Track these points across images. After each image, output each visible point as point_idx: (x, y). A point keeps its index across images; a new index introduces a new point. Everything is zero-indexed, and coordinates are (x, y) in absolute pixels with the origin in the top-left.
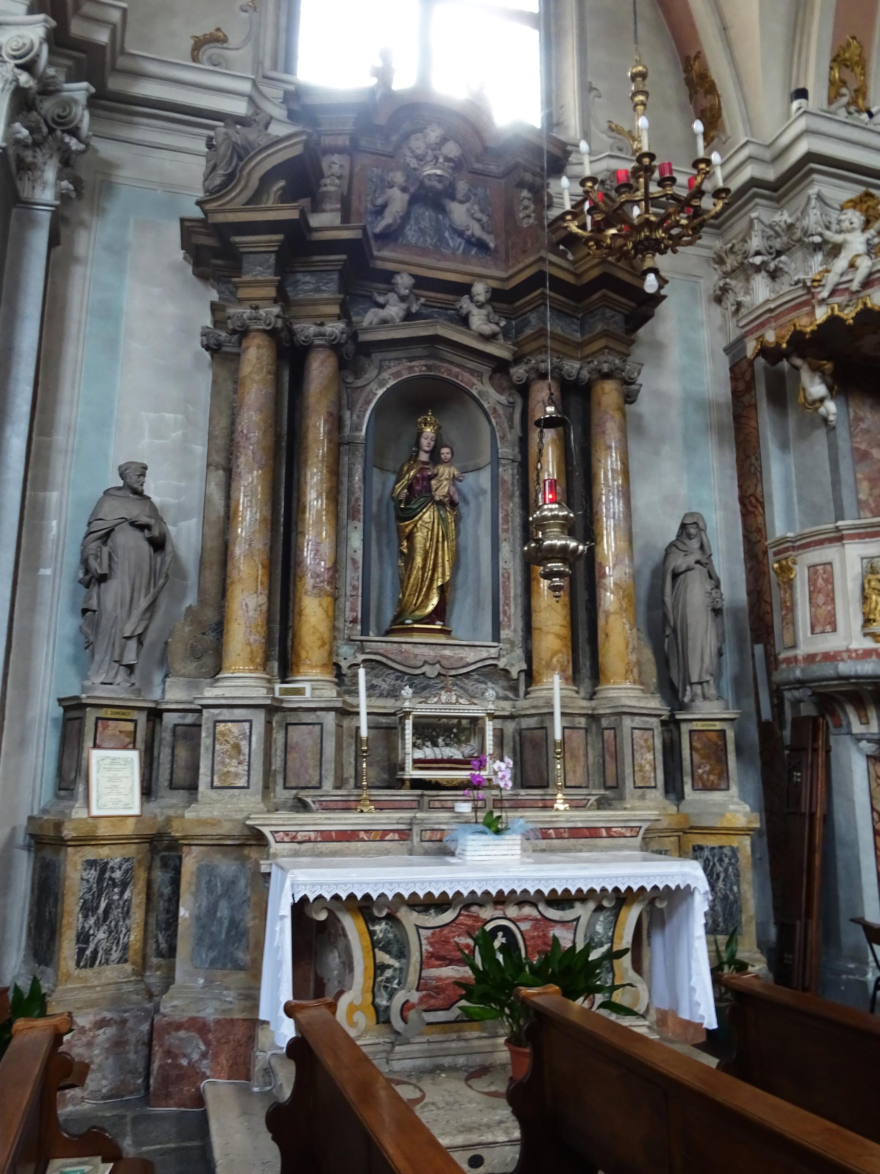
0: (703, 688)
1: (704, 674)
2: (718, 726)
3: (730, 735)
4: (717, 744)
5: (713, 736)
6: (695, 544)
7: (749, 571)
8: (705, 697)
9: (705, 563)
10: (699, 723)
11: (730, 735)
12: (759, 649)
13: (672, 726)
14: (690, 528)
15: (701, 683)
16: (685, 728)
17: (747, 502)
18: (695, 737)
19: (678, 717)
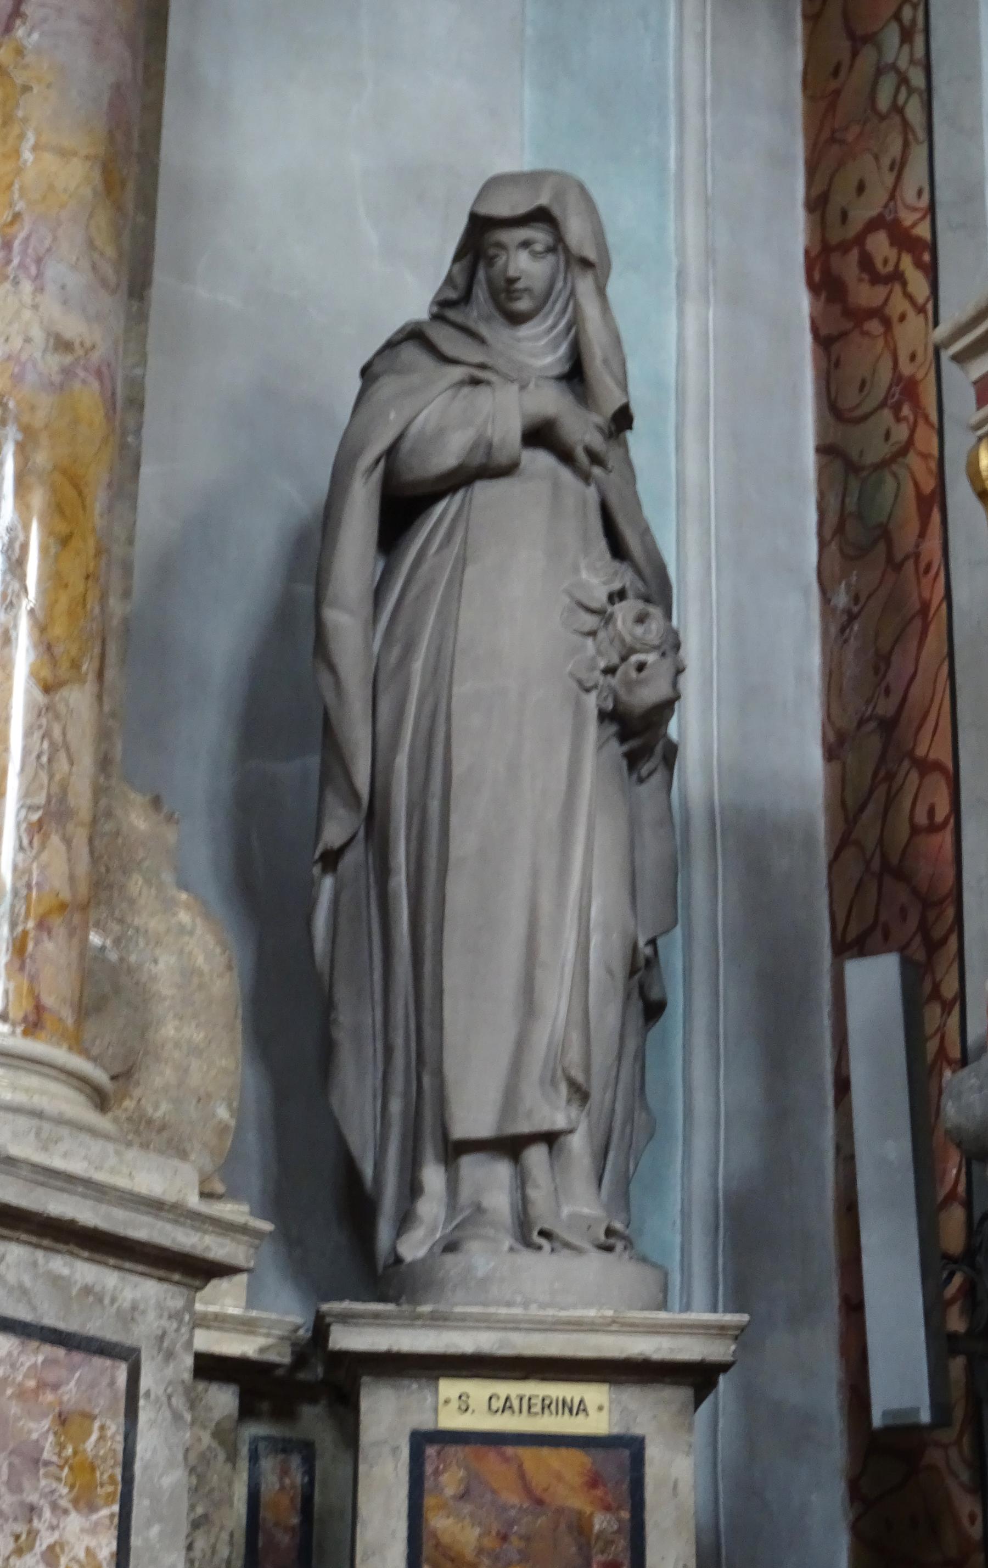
0: (522, 1180)
1: (531, 1093)
2: (596, 1410)
3: (676, 1474)
4: (580, 1527)
5: (563, 1476)
6: (536, 348)
7: (840, 626)
8: (529, 1233)
9: (586, 434)
10: (478, 1390)
11: (676, 1474)
12: (874, 983)
13: (313, 1420)
14: (508, 259)
15: (510, 1147)
16: (387, 1416)
17: (848, 266)
18: (449, 1479)
19: (345, 1339)
